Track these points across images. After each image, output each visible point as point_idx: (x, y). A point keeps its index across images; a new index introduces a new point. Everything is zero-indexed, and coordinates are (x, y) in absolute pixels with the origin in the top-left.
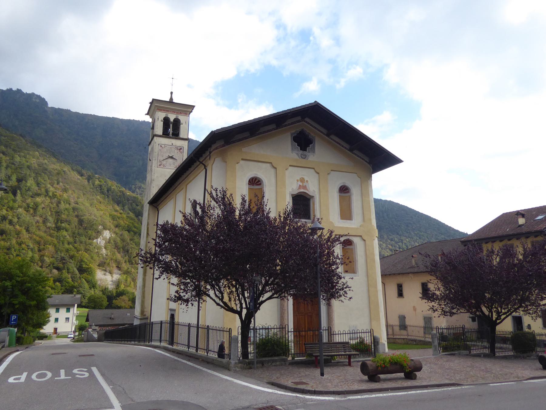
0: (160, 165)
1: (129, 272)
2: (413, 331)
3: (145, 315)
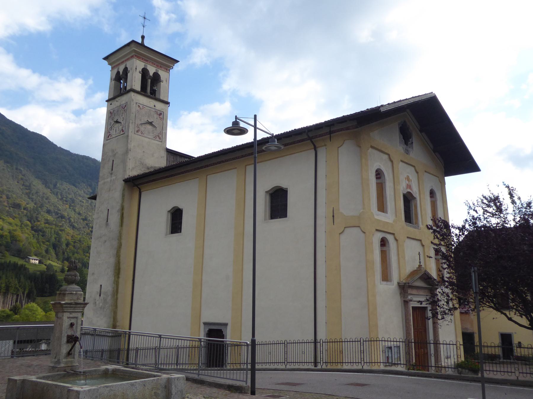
0: (137, 131)
2: (270, 353)
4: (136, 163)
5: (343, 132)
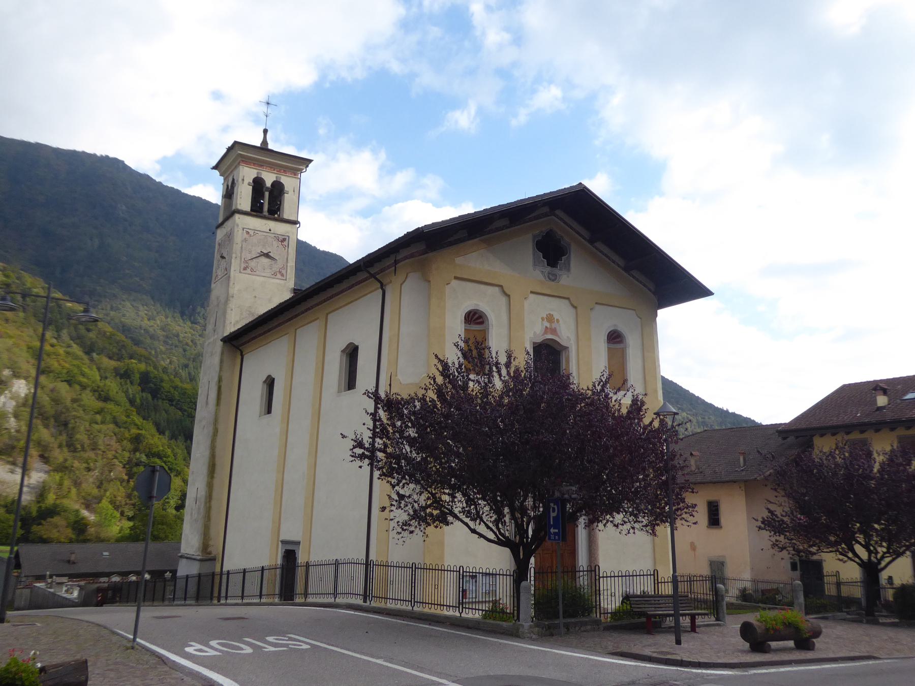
0: (245, 269)
1: (66, 468)
3: (210, 553)
4: (241, 314)
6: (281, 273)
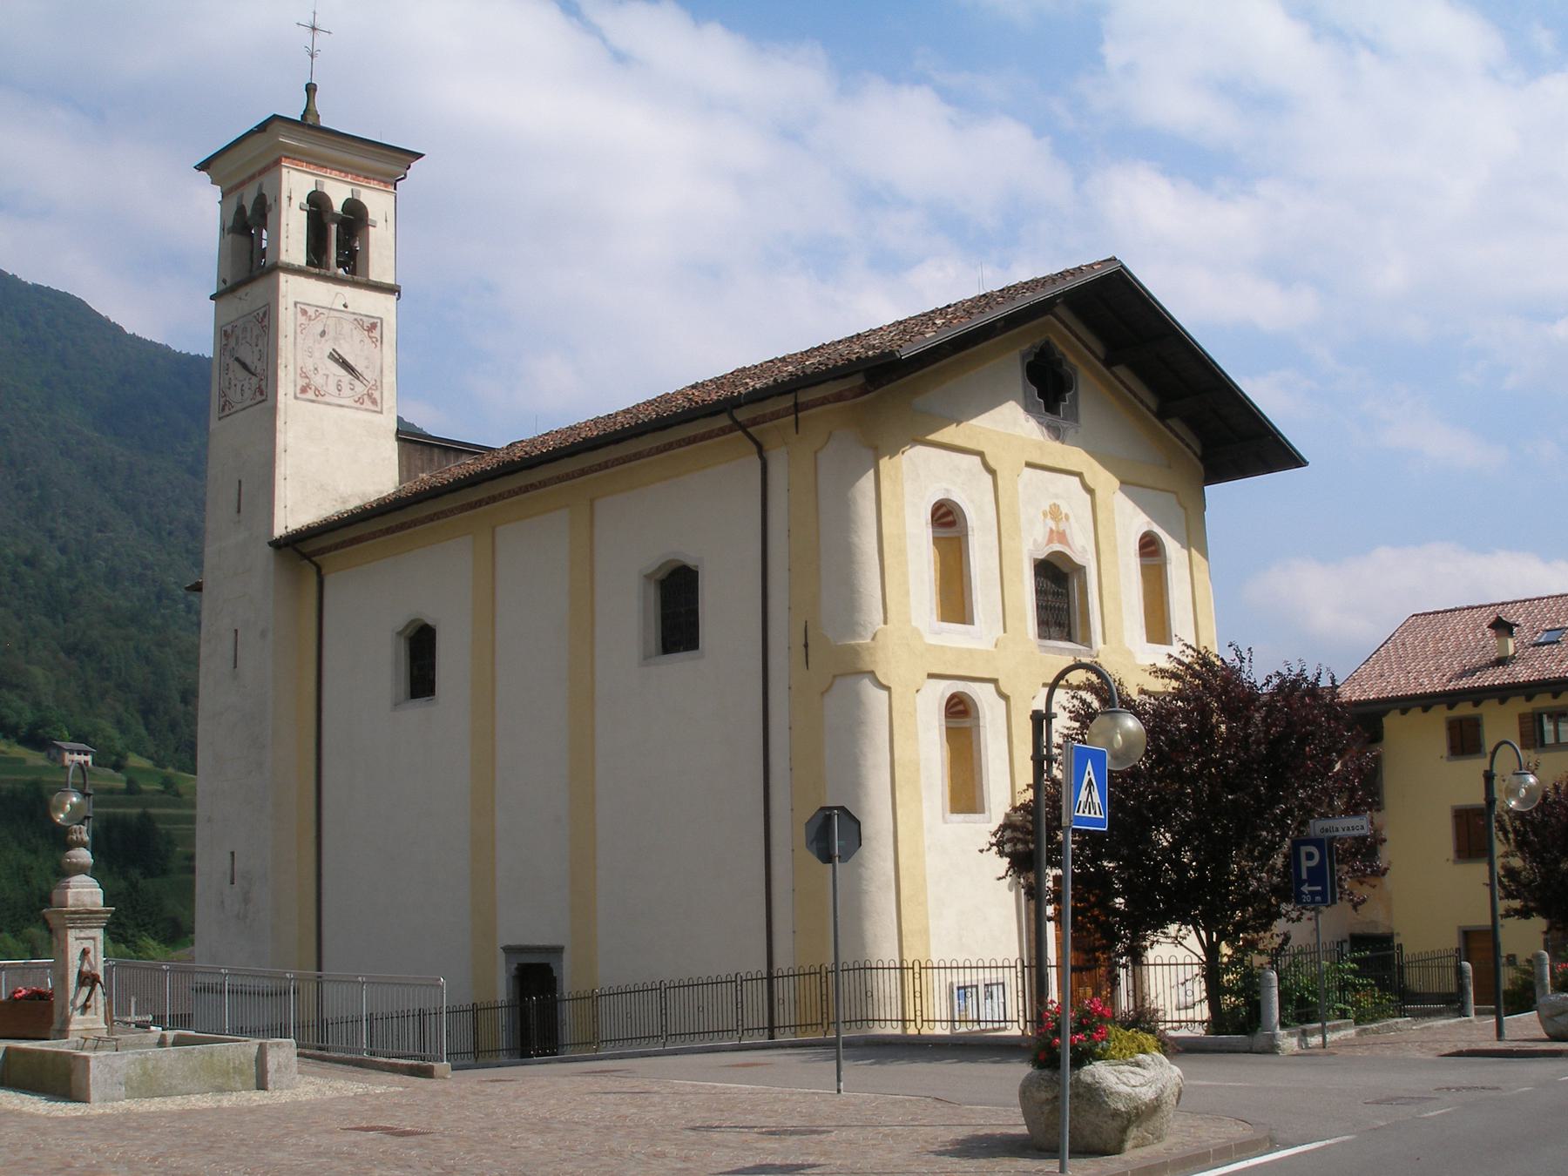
0: (304, 390)
5: (829, 407)
6: (371, 400)
